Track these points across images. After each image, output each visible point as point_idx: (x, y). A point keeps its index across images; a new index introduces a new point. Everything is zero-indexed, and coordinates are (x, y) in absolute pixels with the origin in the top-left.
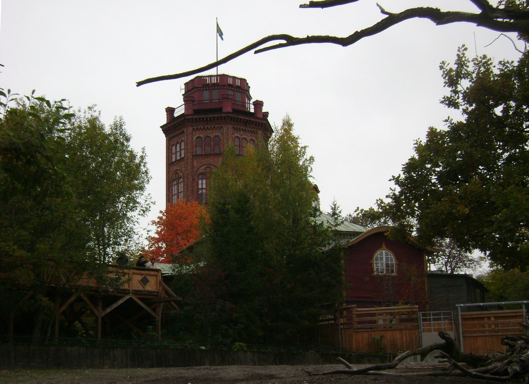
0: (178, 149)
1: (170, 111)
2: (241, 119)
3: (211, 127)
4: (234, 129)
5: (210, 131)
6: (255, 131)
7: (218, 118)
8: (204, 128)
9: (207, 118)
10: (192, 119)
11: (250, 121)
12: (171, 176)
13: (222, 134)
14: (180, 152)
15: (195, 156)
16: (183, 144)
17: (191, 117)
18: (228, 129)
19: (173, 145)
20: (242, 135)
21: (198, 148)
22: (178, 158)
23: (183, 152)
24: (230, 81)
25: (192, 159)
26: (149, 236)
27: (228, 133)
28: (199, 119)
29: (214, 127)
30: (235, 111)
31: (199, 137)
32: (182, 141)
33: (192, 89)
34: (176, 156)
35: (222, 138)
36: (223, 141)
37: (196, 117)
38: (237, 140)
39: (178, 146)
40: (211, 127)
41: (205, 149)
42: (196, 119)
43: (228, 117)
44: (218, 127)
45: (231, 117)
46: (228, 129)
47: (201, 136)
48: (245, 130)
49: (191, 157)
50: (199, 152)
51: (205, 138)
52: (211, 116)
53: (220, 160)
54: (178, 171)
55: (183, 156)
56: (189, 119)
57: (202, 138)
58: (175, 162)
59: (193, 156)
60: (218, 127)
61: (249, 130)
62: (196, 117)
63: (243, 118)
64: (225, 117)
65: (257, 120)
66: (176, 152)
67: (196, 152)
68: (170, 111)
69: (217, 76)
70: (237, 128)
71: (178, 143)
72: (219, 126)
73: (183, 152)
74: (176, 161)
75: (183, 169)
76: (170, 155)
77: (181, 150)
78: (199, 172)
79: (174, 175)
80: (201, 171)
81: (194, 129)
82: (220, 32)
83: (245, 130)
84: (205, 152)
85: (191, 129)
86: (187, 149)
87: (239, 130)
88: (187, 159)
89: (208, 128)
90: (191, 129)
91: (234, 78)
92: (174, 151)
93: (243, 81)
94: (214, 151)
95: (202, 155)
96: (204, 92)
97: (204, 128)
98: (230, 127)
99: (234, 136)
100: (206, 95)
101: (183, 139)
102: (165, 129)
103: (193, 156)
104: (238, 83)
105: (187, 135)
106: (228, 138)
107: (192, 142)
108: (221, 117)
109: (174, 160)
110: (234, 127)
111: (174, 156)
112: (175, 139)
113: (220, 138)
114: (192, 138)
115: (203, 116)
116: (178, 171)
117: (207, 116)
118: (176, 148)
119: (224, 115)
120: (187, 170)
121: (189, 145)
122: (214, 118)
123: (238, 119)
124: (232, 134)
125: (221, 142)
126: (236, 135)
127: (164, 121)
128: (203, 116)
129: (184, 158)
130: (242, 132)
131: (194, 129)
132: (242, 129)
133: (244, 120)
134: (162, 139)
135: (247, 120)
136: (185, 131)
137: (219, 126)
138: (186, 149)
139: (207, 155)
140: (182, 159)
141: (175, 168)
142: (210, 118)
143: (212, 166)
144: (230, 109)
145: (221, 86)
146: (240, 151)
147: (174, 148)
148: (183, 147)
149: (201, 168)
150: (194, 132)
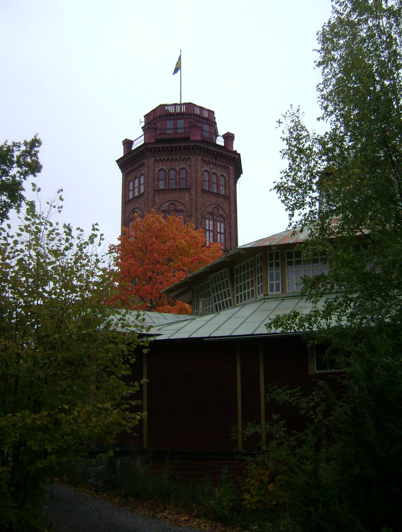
0: (137, 185)
1: (128, 143)
2: (211, 150)
3: (176, 159)
4: (204, 162)
5: (175, 163)
6: (226, 166)
7: (185, 147)
8: (168, 159)
9: (172, 148)
10: (155, 148)
11: (221, 153)
12: (127, 216)
13: (190, 166)
14: (139, 186)
15: (157, 191)
16: (142, 178)
17: (153, 146)
18: (196, 161)
19: (131, 181)
20: (211, 169)
21: (160, 182)
22: (136, 194)
23: (142, 187)
24: (197, 112)
25: (154, 194)
26: (134, 221)
27: (196, 165)
28: (163, 148)
29: (180, 158)
30: (203, 141)
31: (162, 169)
32: (142, 174)
33: (154, 119)
34: (134, 193)
35: (189, 171)
36: (191, 175)
37: (158, 146)
38: (206, 174)
39: (137, 181)
40: (176, 159)
41: (169, 183)
42: (159, 148)
43: (197, 146)
44: (184, 158)
45: (201, 147)
46: (196, 161)
47: (165, 168)
48: (215, 163)
49: (153, 192)
50: (162, 187)
51: (169, 171)
52: (176, 145)
53: (187, 195)
54: (136, 210)
55: (142, 191)
56: (150, 149)
57: (165, 171)
58: (132, 199)
59: (155, 191)
60: (184, 158)
61: (220, 164)
62: (158, 146)
63: (213, 149)
64: (193, 147)
65: (228, 154)
66: (134, 188)
67: (158, 187)
68: (128, 143)
69: (181, 104)
70: (206, 160)
71: (136, 178)
72: (186, 157)
73: (142, 187)
74: (134, 197)
75: (143, 206)
76: (127, 192)
77: (140, 185)
78: (161, 209)
79: (131, 215)
80: (164, 208)
81: (156, 160)
82: (177, 69)
83: (215, 163)
84: (169, 187)
85: (152, 160)
86: (148, 182)
87: (209, 163)
88: (148, 194)
89: (172, 159)
90: (152, 160)
91: (201, 108)
92: (131, 188)
93: (211, 113)
94: (179, 185)
95: (165, 190)
96: (168, 122)
97: (168, 159)
98: (199, 158)
99: (203, 169)
100: (170, 124)
101: (143, 172)
102: (122, 163)
103: (155, 191)
104: (206, 115)
105: (148, 167)
106: (196, 171)
107: (154, 176)
108: (189, 147)
109: (131, 197)
110: (203, 159)
111: (131, 193)
112: (133, 174)
113: (186, 171)
114: (154, 171)
115: (167, 145)
116: (136, 210)
117: (172, 145)
118: (134, 184)
119: (192, 144)
120: (148, 206)
121: (150, 178)
122: (180, 147)
123: (208, 149)
124: (201, 167)
125: (189, 175)
126: (205, 168)
127: (120, 153)
128: (167, 145)
129: (143, 193)
130: (212, 166)
131: (156, 160)
132: (212, 162)
133: (214, 151)
134: (118, 175)
135: (218, 152)
136: (146, 162)
137: (186, 157)
138: (147, 184)
139: (171, 190)
140: (141, 195)
141: (131, 207)
142: (176, 147)
143: (178, 203)
144: (198, 138)
145: (187, 115)
146: (209, 188)
147: (131, 184)
148: (142, 182)
149: (164, 205)
150: (156, 164)
